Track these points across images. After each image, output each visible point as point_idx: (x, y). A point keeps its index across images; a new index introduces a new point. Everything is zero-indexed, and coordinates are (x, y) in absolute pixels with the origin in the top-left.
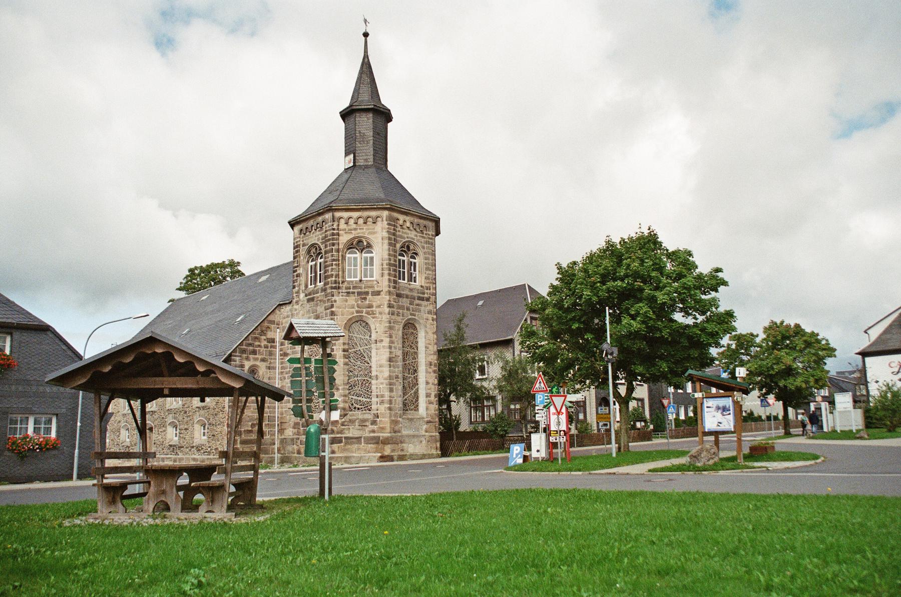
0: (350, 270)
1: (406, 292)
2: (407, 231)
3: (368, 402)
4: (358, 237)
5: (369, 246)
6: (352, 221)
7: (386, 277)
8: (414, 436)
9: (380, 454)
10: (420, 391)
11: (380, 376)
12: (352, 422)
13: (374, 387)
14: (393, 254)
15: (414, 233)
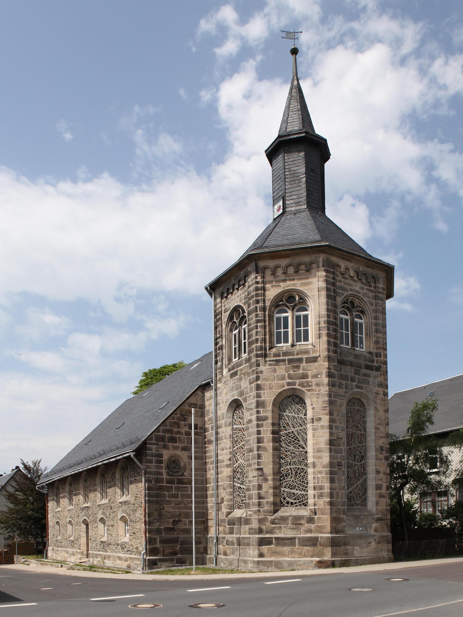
0: (279, 334)
1: (351, 358)
7: (325, 338)
8: (360, 537)
9: (318, 559)
10: (369, 482)
12: (284, 519)
14: (332, 310)
15: (359, 284)
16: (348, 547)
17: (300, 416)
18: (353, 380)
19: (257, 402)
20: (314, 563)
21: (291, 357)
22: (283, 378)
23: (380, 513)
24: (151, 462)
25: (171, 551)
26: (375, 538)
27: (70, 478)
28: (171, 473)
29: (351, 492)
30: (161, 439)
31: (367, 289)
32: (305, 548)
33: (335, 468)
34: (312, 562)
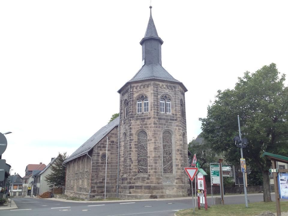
1: (164, 117)
2: (164, 90)
3: (146, 169)
4: (141, 94)
5: (146, 97)
6: (138, 88)
8: (169, 186)
9: (150, 195)
11: (151, 157)
12: (139, 178)
13: (148, 161)
16: (163, 190)
17: (145, 138)
18: (165, 125)
19: (130, 134)
20: (149, 196)
21: (142, 117)
22: (139, 125)
23: (178, 176)
24: (95, 156)
25: (101, 191)
26: (176, 186)
27: (77, 159)
28: (103, 160)
29: (165, 168)
30: (100, 147)
31: (172, 91)
32: (146, 190)
33: (157, 158)
34: (148, 196)
